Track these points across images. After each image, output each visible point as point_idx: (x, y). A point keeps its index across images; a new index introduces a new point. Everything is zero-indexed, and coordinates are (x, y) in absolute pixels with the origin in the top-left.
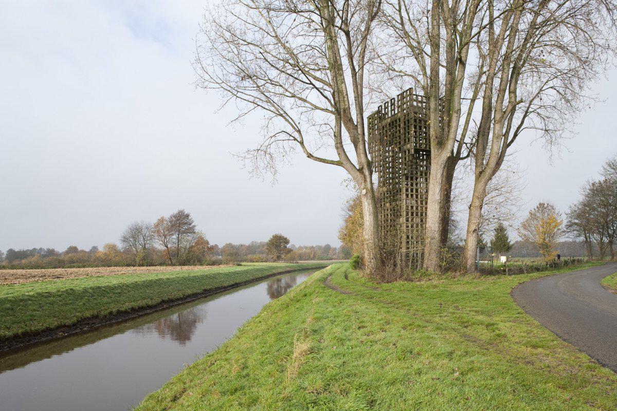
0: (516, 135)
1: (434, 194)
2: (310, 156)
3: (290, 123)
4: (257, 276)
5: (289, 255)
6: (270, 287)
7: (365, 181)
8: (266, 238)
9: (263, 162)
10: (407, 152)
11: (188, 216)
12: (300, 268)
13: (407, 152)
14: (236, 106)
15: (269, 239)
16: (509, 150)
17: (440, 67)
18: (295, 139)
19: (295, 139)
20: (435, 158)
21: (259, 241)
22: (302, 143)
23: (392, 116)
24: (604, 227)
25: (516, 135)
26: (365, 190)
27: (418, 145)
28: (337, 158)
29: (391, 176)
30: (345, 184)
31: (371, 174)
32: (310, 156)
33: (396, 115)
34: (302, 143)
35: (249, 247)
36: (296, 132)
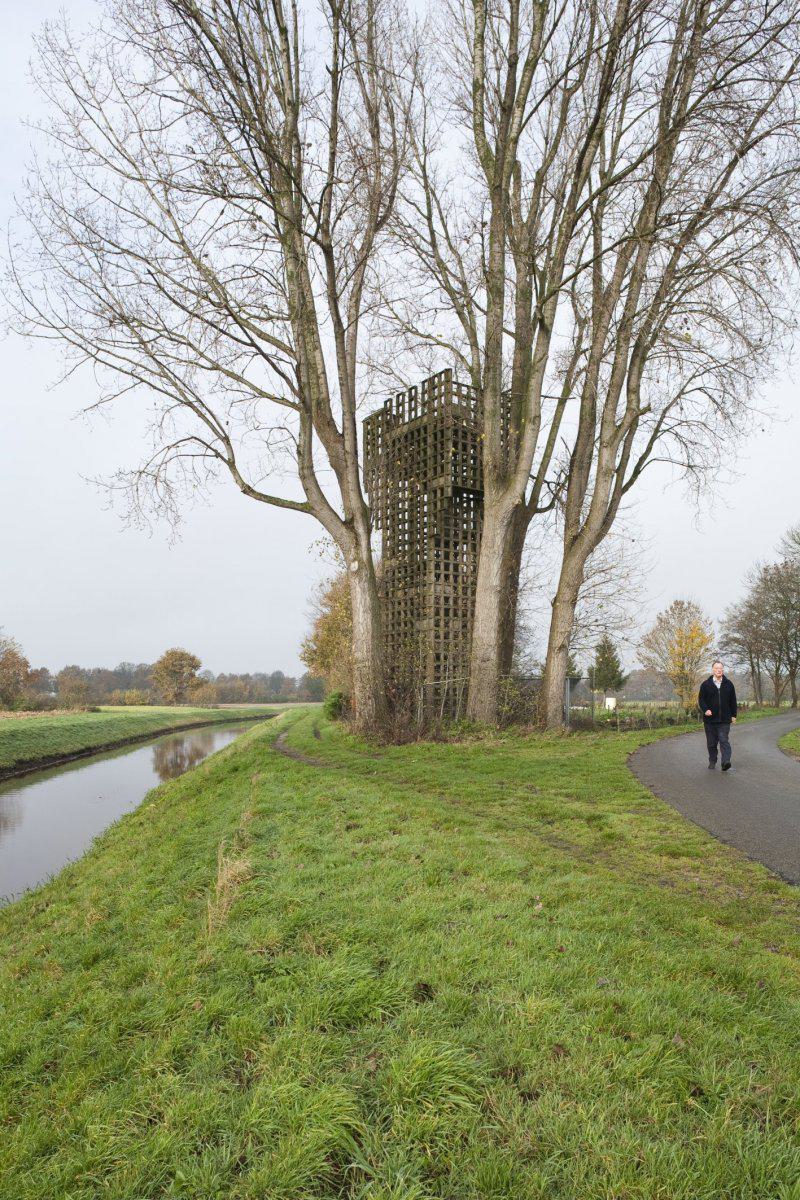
0: (637, 472)
1: (488, 577)
2: (247, 490)
3: (207, 421)
4: (133, 734)
6: (160, 757)
7: (357, 544)
9: (150, 497)
10: (439, 492)
13: (439, 492)
14: (95, 380)
16: (625, 500)
18: (218, 455)
19: (218, 455)
21: (137, 662)
22: (231, 464)
23: (411, 420)
24: (780, 645)
25: (637, 472)
26: (357, 563)
28: (302, 498)
30: (317, 549)
32: (247, 490)
34: (231, 464)
35: (115, 673)
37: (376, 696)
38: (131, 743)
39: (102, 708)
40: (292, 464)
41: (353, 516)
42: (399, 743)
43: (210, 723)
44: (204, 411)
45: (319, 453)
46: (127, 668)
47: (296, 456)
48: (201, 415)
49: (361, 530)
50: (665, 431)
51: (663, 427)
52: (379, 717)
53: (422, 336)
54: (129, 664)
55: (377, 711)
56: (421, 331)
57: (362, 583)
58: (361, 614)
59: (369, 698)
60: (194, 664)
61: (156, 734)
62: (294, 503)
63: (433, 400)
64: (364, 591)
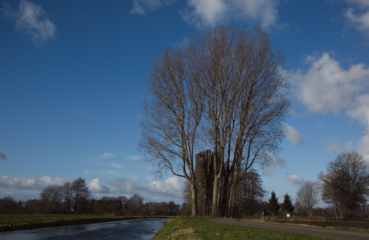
11: (84, 181)
28: (183, 175)
32: (174, 174)
34: (171, 169)
40: (182, 169)
45: (187, 166)
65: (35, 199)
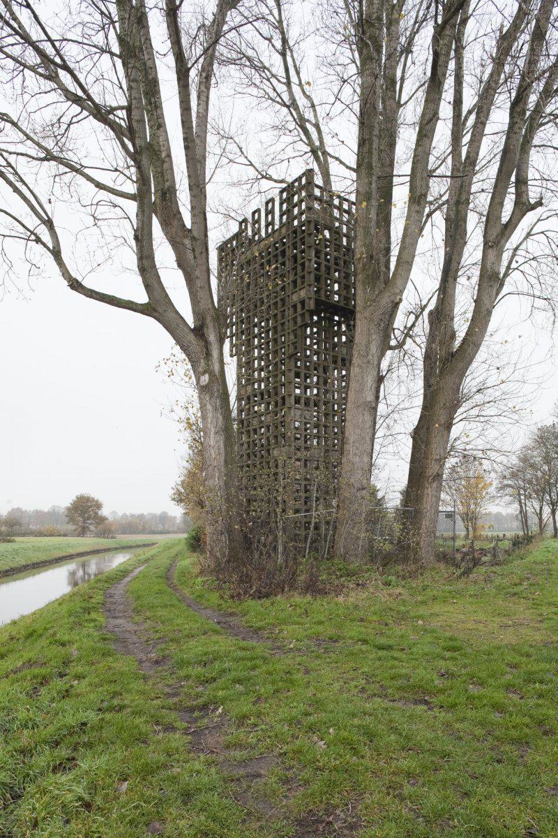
1: (361, 390)
2: (75, 285)
4: (35, 560)
5: (101, 527)
6: (73, 574)
7: (208, 355)
8: (65, 501)
10: (299, 306)
12: (118, 546)
13: (299, 306)
15: (71, 502)
17: (355, 167)
18: (38, 240)
19: (38, 240)
20: (365, 308)
22: (56, 253)
23: (268, 236)
24: (542, 489)
26: (207, 376)
27: (322, 293)
28: (142, 298)
29: (263, 387)
30: (165, 369)
31: (221, 342)
32: (75, 285)
33: (277, 234)
34: (56, 253)
35: (49, 513)
36: (43, 226)
37: (230, 531)
38: (34, 568)
39: (17, 539)
41: (204, 319)
42: (260, 595)
43: (109, 550)
44: (19, 185)
45: (164, 254)
46: (56, 509)
47: (133, 243)
48: (16, 190)
49: (212, 337)
50: (515, 269)
51: (514, 265)
52: (233, 558)
53: (276, 181)
54: (58, 507)
55: (231, 549)
56: (275, 177)
57: (213, 400)
58: (212, 435)
59: (222, 534)
60: (99, 506)
61: (131, 547)
62: (132, 302)
63: (293, 196)
64: (215, 409)
65: (18, 509)
